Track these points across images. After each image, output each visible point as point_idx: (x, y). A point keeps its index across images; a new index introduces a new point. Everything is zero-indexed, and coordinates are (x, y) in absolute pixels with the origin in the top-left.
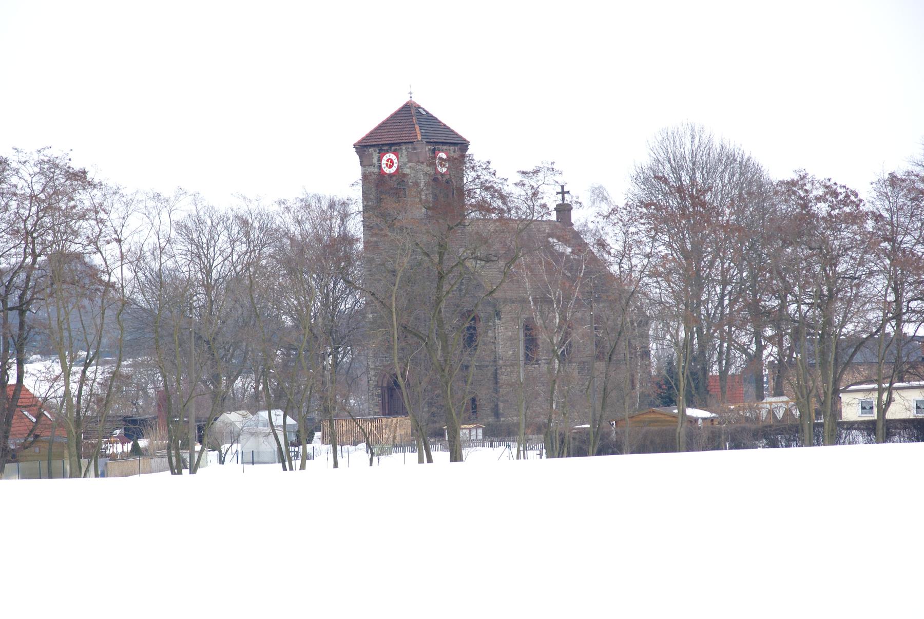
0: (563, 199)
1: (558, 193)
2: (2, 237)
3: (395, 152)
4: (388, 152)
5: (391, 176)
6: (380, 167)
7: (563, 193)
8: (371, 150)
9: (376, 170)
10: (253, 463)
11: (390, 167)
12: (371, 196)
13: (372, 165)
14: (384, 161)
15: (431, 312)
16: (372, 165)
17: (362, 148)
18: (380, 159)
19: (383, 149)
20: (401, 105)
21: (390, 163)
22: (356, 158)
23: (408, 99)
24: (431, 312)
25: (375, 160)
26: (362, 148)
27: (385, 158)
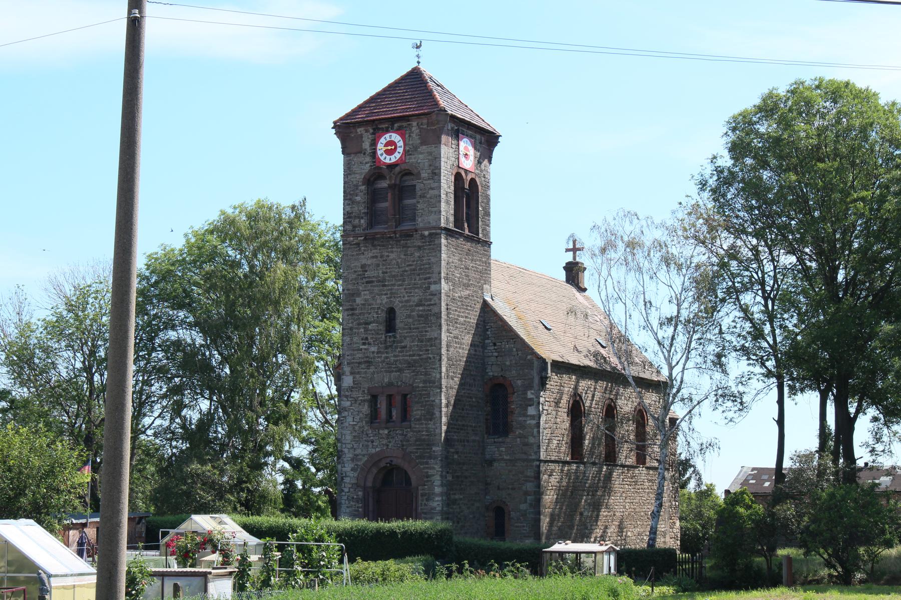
0: (574, 258)
1: (567, 250)
2: (248, 597)
3: (399, 131)
4: (387, 131)
5: (391, 166)
6: (374, 154)
7: (575, 250)
8: (360, 130)
9: (368, 159)
10: (74, 586)
11: (390, 152)
12: (358, 198)
13: (361, 152)
14: (381, 147)
15: (781, 422)
16: (361, 152)
17: (346, 128)
18: (374, 144)
19: (378, 127)
20: (404, 72)
21: (391, 149)
22: (337, 144)
23: (415, 65)
24: (781, 422)
25: (366, 145)
26: (346, 128)
27: (383, 141)
